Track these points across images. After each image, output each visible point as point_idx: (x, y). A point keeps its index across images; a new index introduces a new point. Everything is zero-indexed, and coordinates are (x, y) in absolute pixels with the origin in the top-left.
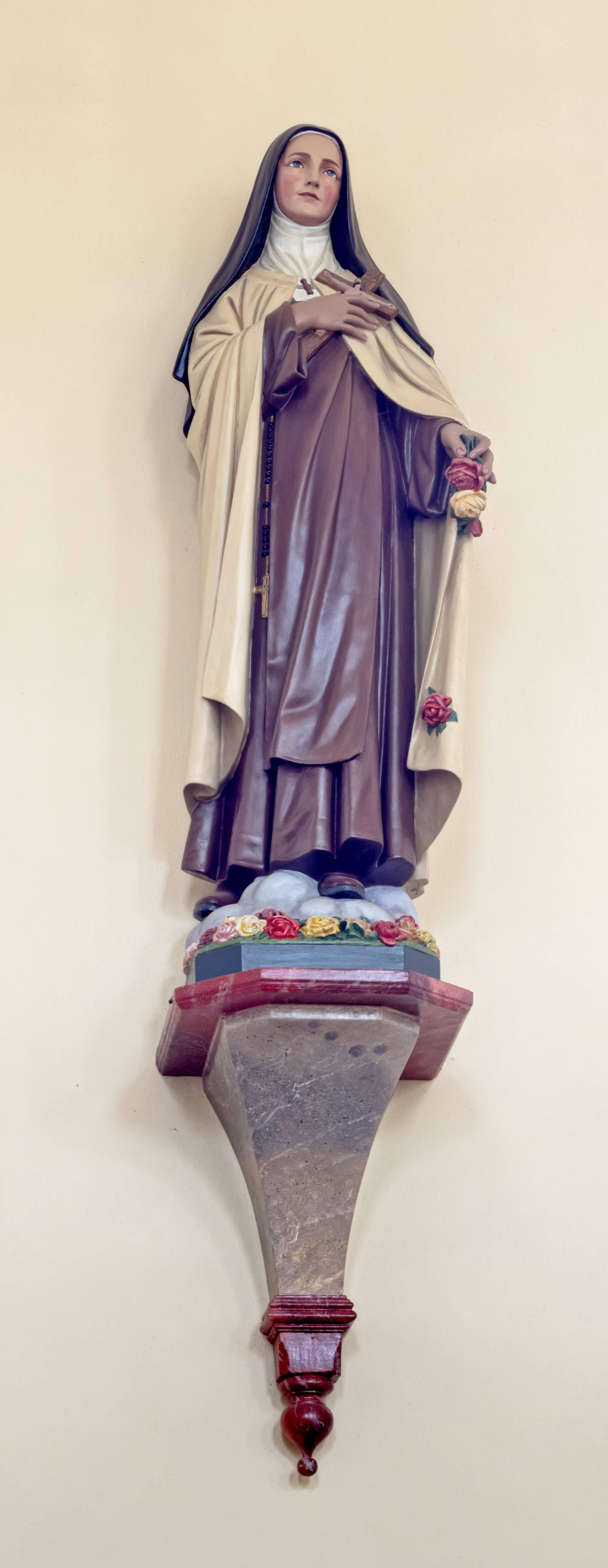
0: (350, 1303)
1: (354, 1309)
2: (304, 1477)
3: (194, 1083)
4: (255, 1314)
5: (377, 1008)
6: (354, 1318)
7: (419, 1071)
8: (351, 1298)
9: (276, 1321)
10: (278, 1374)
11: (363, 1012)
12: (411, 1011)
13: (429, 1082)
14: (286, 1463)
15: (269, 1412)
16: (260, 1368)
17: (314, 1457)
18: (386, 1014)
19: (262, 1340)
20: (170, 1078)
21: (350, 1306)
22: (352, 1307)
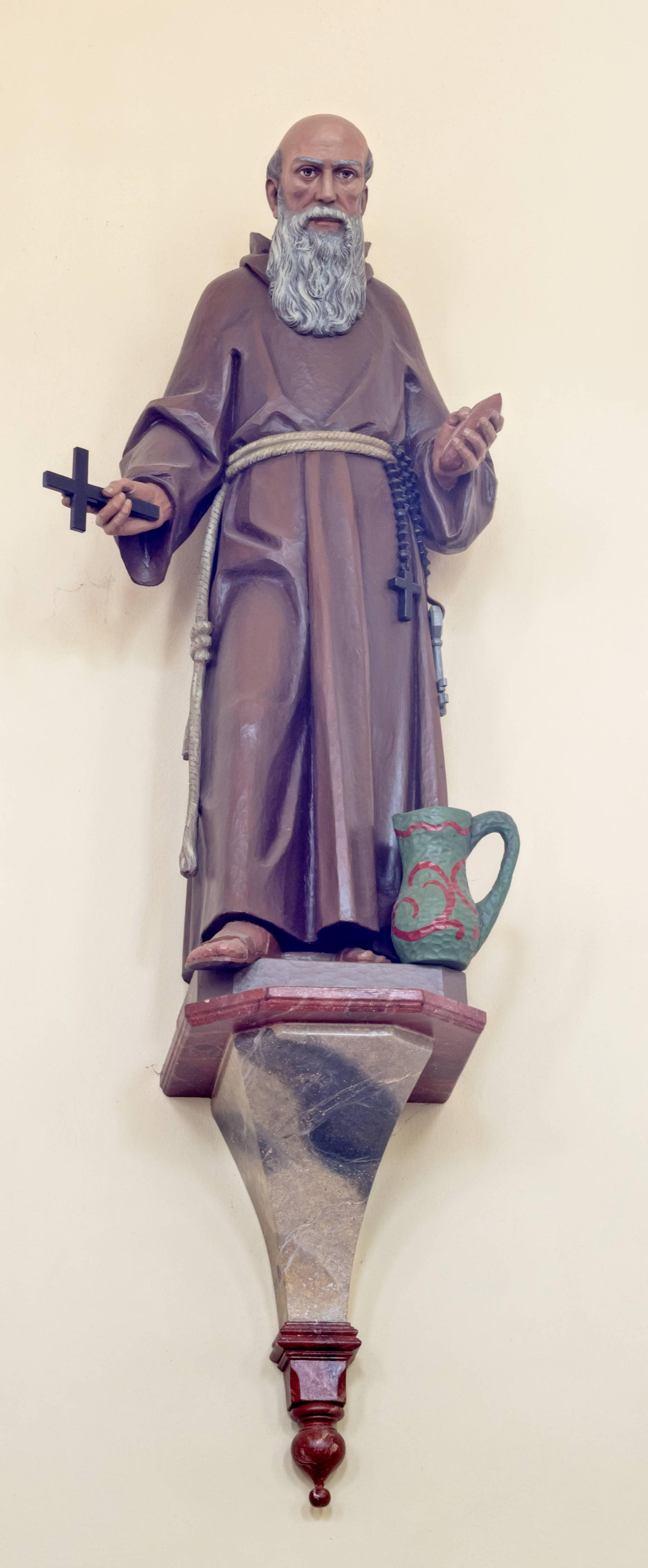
0: (353, 1329)
1: (358, 1337)
2: (317, 1509)
3: (201, 1108)
4: (270, 1333)
5: (389, 1026)
6: (357, 1345)
7: (430, 1092)
8: (354, 1325)
9: (286, 1347)
10: (290, 1403)
11: (372, 1029)
12: (424, 1030)
13: (441, 1105)
14: (300, 1490)
15: (282, 1434)
16: (273, 1390)
17: (327, 1486)
18: (397, 1032)
19: (273, 1367)
20: (172, 1098)
21: (352, 1333)
22: (355, 1334)
